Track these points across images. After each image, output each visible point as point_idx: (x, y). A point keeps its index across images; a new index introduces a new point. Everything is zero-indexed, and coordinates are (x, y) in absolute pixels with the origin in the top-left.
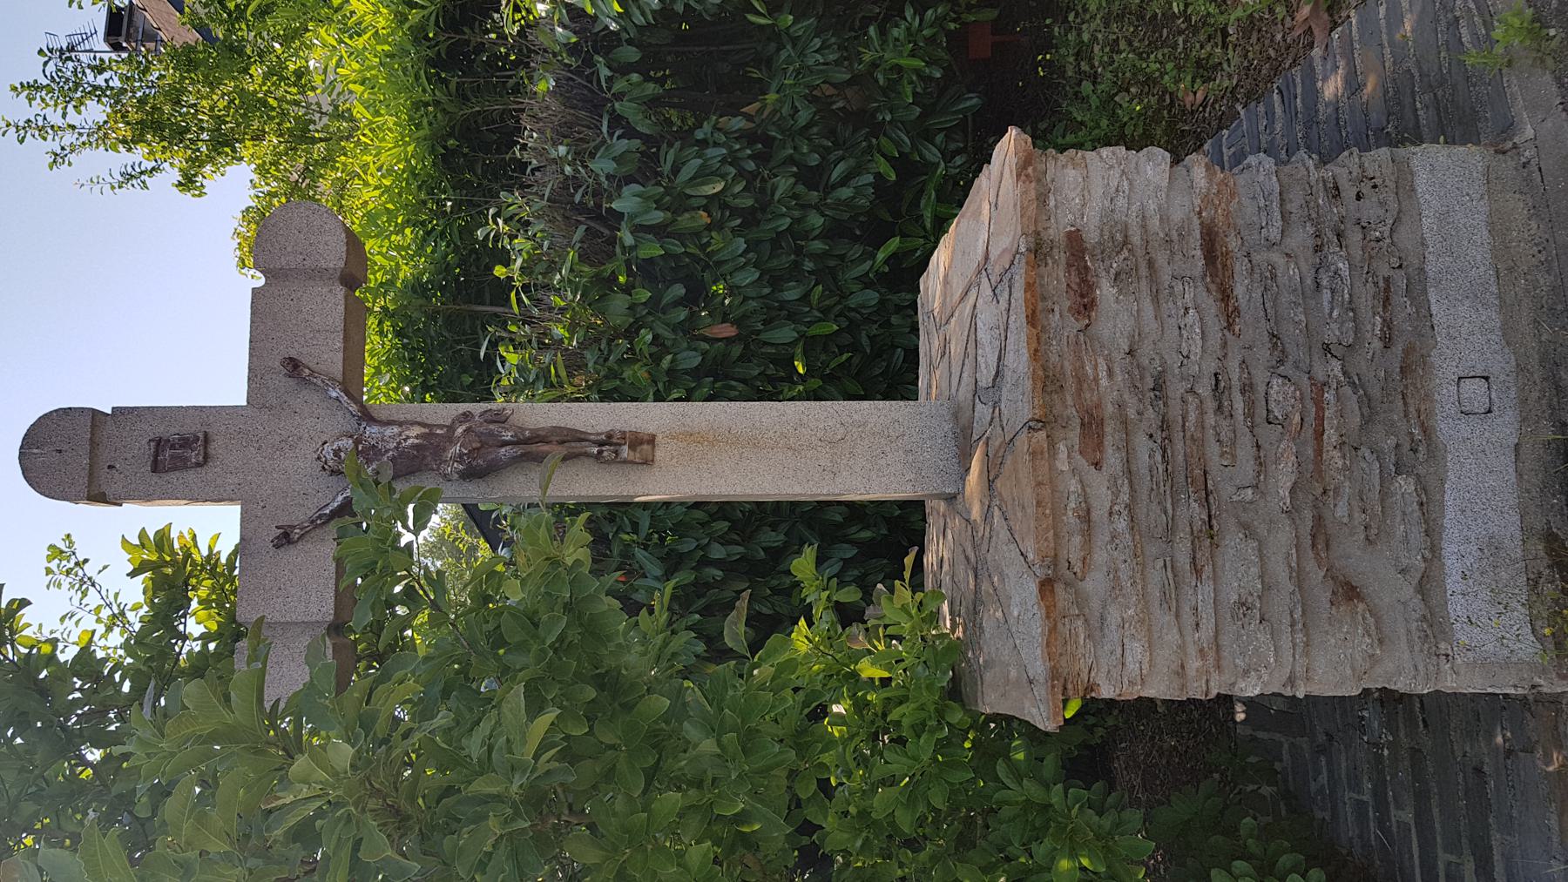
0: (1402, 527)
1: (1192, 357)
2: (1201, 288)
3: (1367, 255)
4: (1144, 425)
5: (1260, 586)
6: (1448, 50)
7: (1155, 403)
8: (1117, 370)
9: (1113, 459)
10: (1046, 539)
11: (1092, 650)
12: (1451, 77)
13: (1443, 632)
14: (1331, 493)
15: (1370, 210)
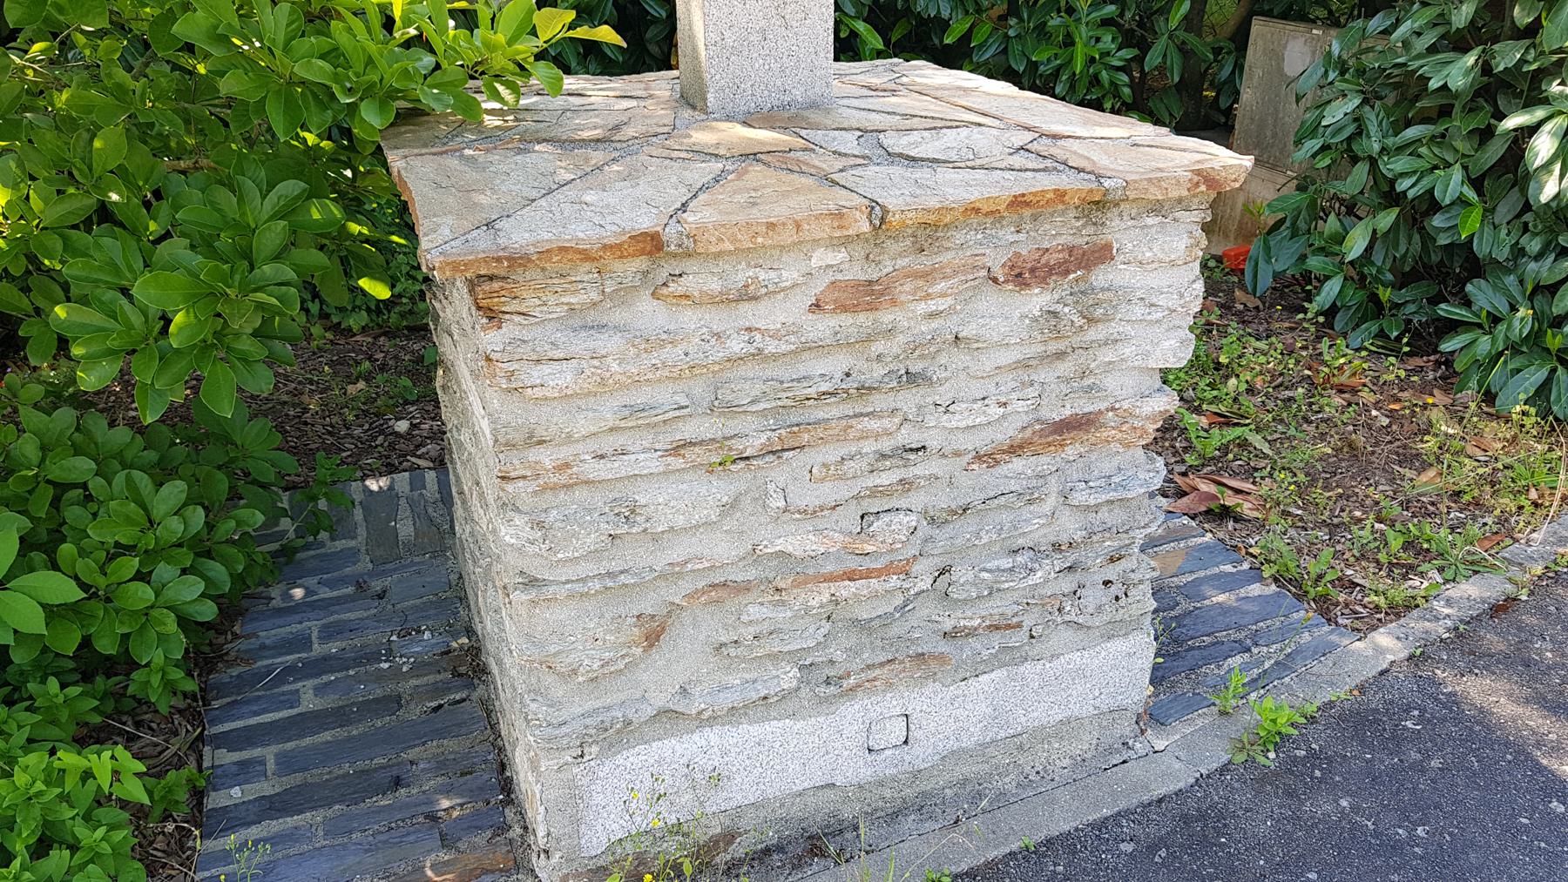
0: (738, 682)
1: (945, 417)
2: (1026, 419)
3: (1048, 600)
4: (862, 364)
5: (660, 530)
6: (1214, 644)
7: (894, 376)
8: (935, 324)
9: (823, 327)
10: (720, 240)
11: (555, 316)
12: (1186, 651)
13: (611, 745)
14: (778, 598)
15: (1094, 596)
